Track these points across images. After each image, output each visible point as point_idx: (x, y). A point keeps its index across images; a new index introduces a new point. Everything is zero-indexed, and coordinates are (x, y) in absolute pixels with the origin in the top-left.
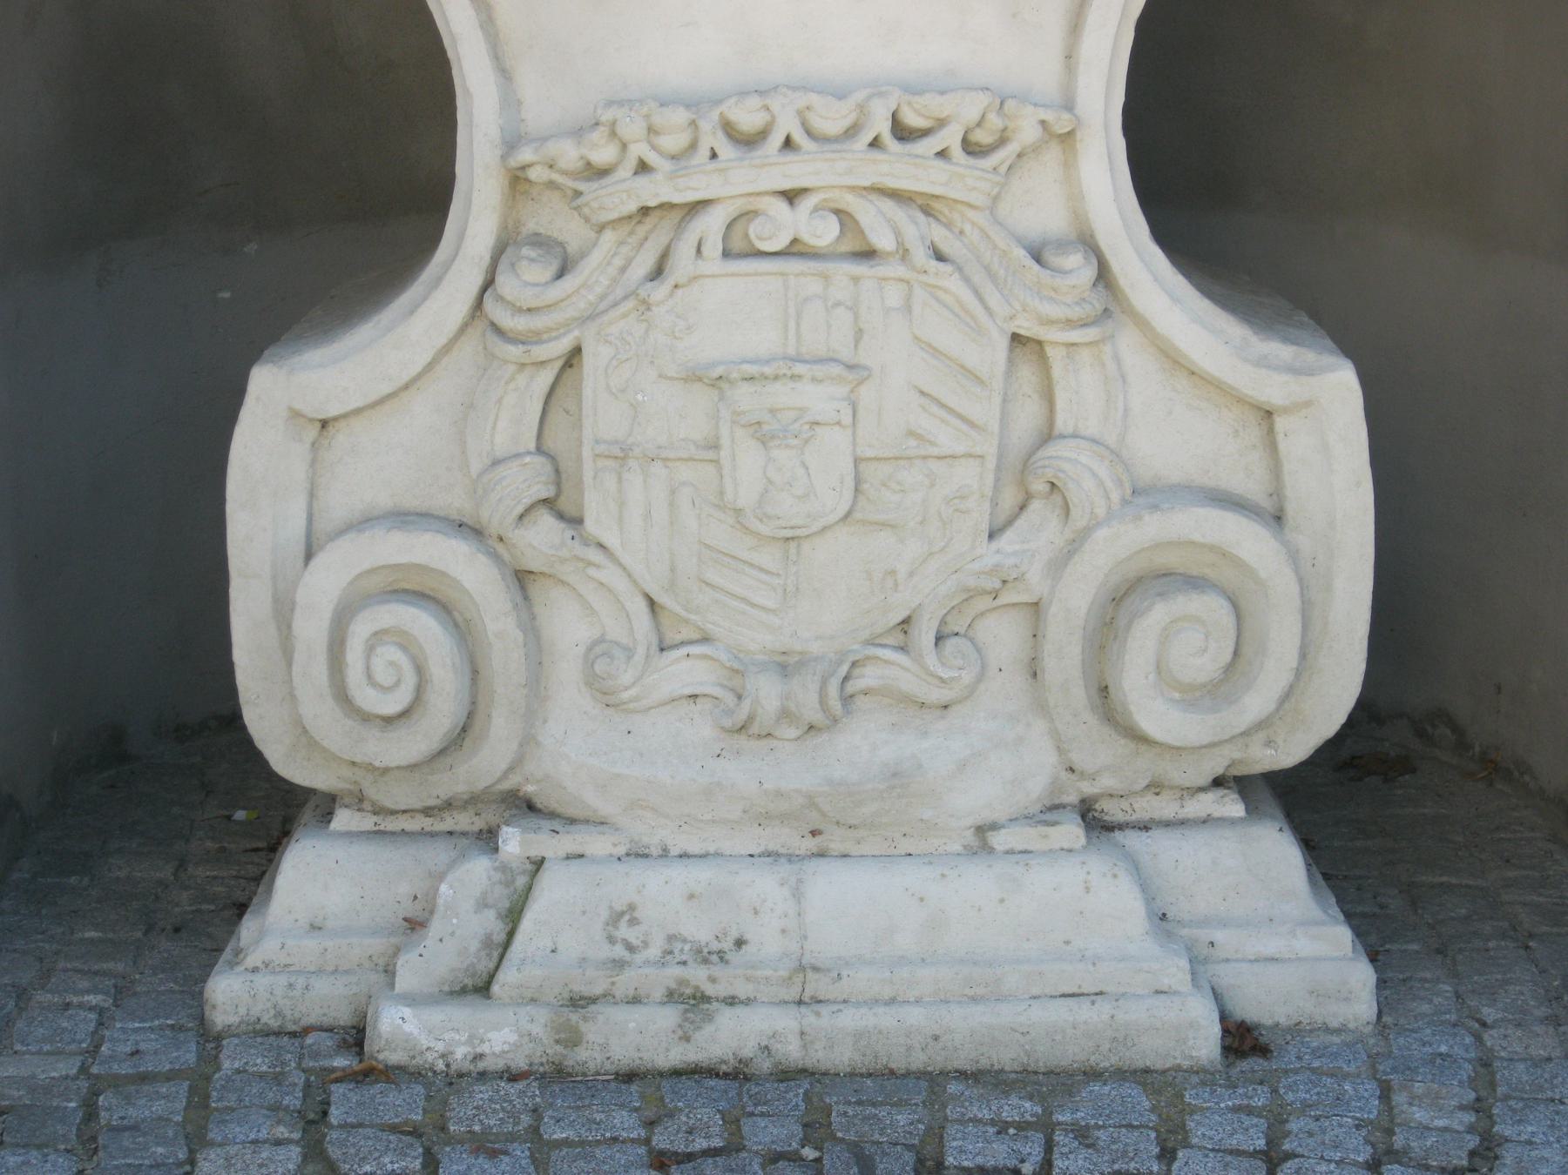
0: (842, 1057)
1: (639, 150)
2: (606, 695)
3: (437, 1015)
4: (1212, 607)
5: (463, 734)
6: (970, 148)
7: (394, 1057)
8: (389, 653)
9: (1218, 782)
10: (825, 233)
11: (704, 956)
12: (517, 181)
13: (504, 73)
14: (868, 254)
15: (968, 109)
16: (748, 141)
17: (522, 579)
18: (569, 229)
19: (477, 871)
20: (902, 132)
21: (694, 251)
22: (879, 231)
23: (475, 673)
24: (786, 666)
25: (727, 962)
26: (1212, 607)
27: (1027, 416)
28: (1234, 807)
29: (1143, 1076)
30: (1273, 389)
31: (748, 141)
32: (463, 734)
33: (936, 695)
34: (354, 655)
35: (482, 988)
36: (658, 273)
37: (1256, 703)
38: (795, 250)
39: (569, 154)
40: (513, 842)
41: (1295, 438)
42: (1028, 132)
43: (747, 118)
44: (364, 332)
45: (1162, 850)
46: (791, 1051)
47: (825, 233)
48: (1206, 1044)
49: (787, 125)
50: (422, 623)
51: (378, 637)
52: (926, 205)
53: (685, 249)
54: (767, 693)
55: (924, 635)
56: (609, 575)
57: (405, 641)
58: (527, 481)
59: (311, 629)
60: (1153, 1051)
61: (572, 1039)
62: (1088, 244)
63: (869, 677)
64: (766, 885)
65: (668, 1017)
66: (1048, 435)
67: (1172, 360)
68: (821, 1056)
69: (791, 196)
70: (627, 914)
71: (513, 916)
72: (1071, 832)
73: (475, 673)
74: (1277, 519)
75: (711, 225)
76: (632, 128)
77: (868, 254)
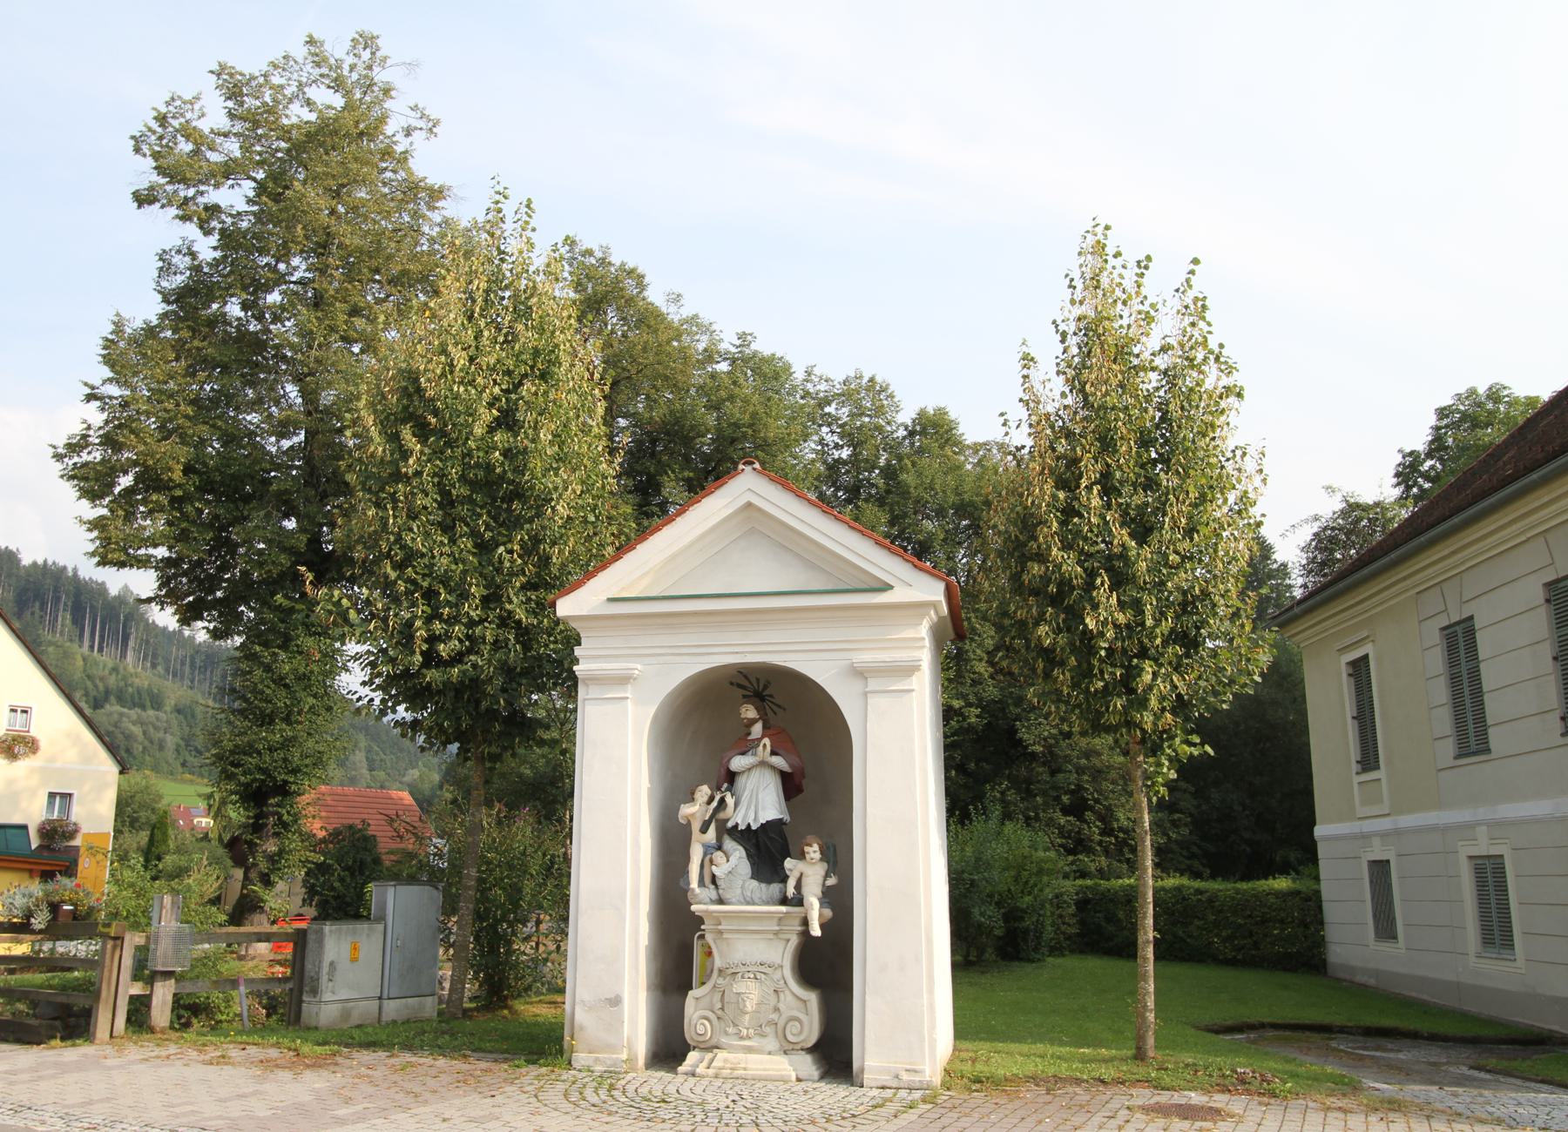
37: (802, 1038)
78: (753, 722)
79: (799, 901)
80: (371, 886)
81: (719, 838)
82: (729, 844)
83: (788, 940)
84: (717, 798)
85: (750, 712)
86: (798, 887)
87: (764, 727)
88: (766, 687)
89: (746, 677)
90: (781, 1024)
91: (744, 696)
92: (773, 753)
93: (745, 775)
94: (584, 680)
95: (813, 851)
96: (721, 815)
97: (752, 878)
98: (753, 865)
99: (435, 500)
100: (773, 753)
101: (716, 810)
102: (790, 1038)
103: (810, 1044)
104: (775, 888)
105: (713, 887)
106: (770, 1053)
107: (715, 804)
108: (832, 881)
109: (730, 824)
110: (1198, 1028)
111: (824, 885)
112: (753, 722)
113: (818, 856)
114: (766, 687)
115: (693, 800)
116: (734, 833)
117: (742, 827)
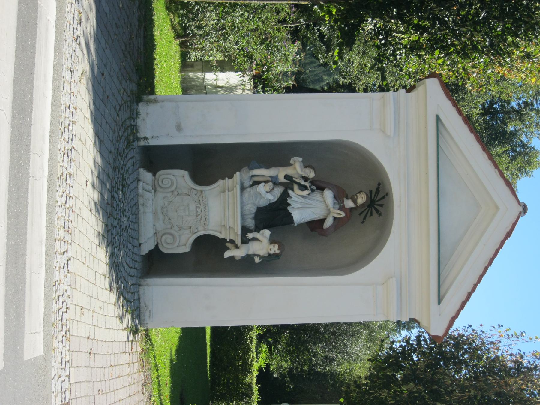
0: (140, 216)
1: (204, 200)
2: (164, 198)
3: (142, 186)
4: (172, 241)
5: (161, 187)
6: (204, 223)
7: (139, 183)
8: (167, 182)
9: (157, 243)
10: (199, 213)
11: (146, 205)
12: (202, 191)
13: (209, 190)
14: (197, 216)
15: (207, 223)
16: (205, 208)
17: (173, 192)
18: (198, 195)
19: (151, 189)
20: (206, 219)
21: (360, 213)
22: (199, 217)
23: (166, 188)
24: (167, 211)
25: (383, 205)
26: (172, 241)
27: (185, 228)
28: (156, 244)
29: (139, 238)
30: (187, 245)
31: (205, 208)
32: (161, 187)
33: (165, 222)
34: (168, 180)
35: (143, 189)
36: (195, 201)
37: (165, 245)
38: (197, 211)
39: (204, 195)
40: (153, 191)
41: (184, 247)
42: (206, 227)
43: (207, 208)
44: (190, 180)
45: (153, 239)
46: (140, 212)
47: (199, 213)
48: (141, 242)
49: (206, 211)
50: (169, 185)
51: (168, 181)
52: (201, 220)
53: (197, 203)
54: (165, 210)
55: (169, 221)
56: (173, 198)
57: (169, 183)
58: (180, 192)
59: (169, 176)
60: (140, 239)
61: (140, 196)
62: (198, 232)
63: (166, 217)
64: (151, 210)
65: (142, 203)
66: (184, 229)
67: (189, 238)
68: (139, 214)
69: (201, 211)
70: (149, 200)
71: (148, 191)
72: (155, 232)
73: (166, 188)
74: (178, 246)
75: (199, 205)
76: (206, 200)
77: (197, 216)
78: (355, 202)
79: (245, 241)
80: (247, 167)
81: (281, 184)
82: (278, 191)
83: (221, 233)
84: (307, 184)
85: (361, 199)
86: (255, 239)
87: (351, 209)
88: (377, 211)
89: (383, 198)
90: (172, 231)
91: (371, 192)
92: (335, 218)
93: (321, 199)
94: (383, 97)
95: (275, 249)
96: (296, 187)
97: (258, 208)
98: (266, 207)
99: (501, 148)
100: (335, 218)
101: (299, 184)
102: (164, 238)
103: (161, 248)
104: (250, 223)
105: (251, 183)
106: (154, 225)
107: (303, 183)
108: (257, 260)
109: (290, 192)
110: (181, 395)
111: (255, 255)
112: (355, 202)
113: (272, 252)
114: (377, 211)
115: (305, 167)
116: (285, 196)
117: (289, 201)
